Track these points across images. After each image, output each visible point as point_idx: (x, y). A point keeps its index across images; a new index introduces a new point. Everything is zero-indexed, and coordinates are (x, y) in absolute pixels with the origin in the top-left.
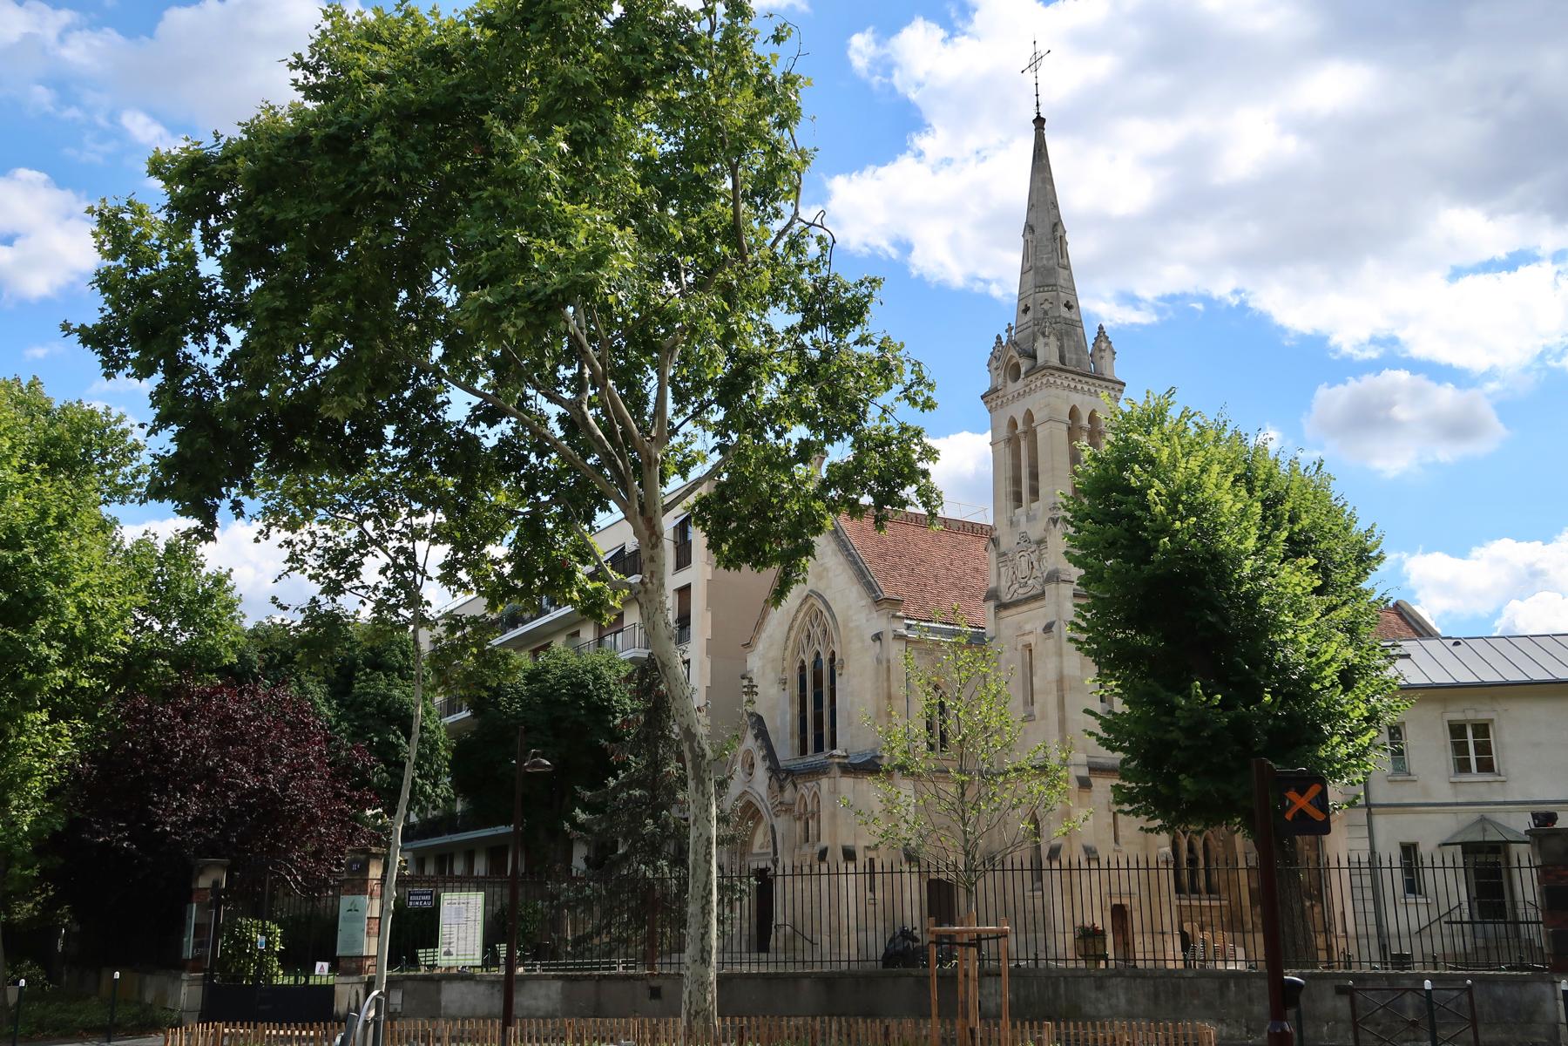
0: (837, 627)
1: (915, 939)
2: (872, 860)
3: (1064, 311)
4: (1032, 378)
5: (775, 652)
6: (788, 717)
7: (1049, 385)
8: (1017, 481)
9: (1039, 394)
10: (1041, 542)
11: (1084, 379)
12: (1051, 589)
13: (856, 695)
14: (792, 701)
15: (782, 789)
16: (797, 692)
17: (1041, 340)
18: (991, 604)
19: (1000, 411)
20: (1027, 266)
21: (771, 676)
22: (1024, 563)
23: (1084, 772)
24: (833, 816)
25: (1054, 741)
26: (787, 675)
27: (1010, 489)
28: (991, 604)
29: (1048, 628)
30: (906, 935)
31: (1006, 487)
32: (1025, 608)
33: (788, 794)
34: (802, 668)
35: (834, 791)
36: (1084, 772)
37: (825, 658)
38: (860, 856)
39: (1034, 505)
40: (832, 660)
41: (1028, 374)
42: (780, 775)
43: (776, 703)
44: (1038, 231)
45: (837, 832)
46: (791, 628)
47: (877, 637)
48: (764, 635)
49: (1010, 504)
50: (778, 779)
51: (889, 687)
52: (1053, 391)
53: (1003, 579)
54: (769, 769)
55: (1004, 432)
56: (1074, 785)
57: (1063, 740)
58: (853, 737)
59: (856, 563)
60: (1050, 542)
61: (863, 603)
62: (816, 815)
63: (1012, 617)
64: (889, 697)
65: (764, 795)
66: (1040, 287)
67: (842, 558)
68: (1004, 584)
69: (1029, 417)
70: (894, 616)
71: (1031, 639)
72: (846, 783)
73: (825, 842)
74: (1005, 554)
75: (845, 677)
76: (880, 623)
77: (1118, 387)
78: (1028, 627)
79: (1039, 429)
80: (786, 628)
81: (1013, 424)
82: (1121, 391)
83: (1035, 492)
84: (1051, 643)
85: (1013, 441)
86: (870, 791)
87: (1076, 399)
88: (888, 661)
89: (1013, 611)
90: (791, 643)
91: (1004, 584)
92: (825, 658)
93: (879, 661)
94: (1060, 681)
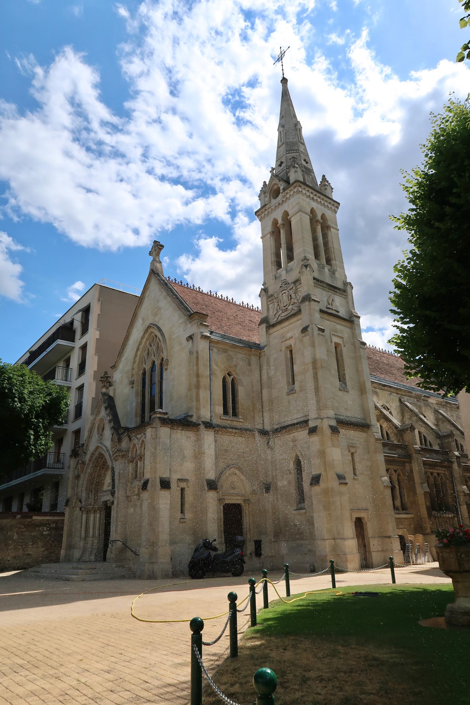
0: (165, 340)
1: (215, 549)
2: (183, 490)
3: (304, 163)
4: (288, 191)
5: (129, 367)
6: (134, 404)
7: (299, 192)
8: (278, 255)
9: (292, 200)
10: (297, 281)
11: (318, 195)
12: (305, 306)
13: (176, 381)
14: (137, 394)
15: (120, 440)
16: (140, 388)
17: (293, 170)
18: (264, 326)
19: (267, 218)
20: (280, 143)
21: (126, 381)
22: (285, 297)
23: (334, 423)
24: (154, 456)
25: (312, 402)
26: (135, 378)
27: (274, 259)
28: (264, 326)
29: (305, 330)
30: (207, 545)
31: (271, 258)
32: (286, 323)
33: (124, 444)
34: (144, 374)
35: (156, 437)
36: (334, 423)
37: (157, 363)
38: (173, 485)
39: (290, 264)
40: (161, 364)
41: (284, 190)
42: (119, 430)
43: (125, 393)
44: (286, 127)
45: (153, 469)
46: (138, 350)
47: (190, 338)
48: (123, 359)
49: (274, 268)
50: (119, 435)
51: (198, 369)
52: (300, 195)
53: (271, 311)
54: (113, 428)
55: (269, 228)
56: (328, 432)
57: (318, 402)
58: (172, 406)
59: (178, 298)
60: (303, 279)
61: (182, 320)
62: (141, 457)
63: (277, 332)
64: (198, 376)
65: (109, 448)
66: (288, 151)
67: (169, 299)
68: (271, 314)
69: (286, 214)
70: (201, 324)
71: (291, 342)
72: (164, 431)
73: (147, 476)
74: (272, 295)
75: (169, 370)
76: (193, 329)
77: (336, 204)
78: (289, 335)
79: (292, 219)
80: (135, 350)
81: (275, 222)
82: (338, 208)
83: (290, 258)
84: (307, 339)
85: (276, 232)
86: (184, 438)
87: (314, 205)
88: (197, 353)
89: (278, 327)
90: (137, 359)
91: (271, 314)
92: (157, 363)
93: (191, 353)
94: (314, 362)
